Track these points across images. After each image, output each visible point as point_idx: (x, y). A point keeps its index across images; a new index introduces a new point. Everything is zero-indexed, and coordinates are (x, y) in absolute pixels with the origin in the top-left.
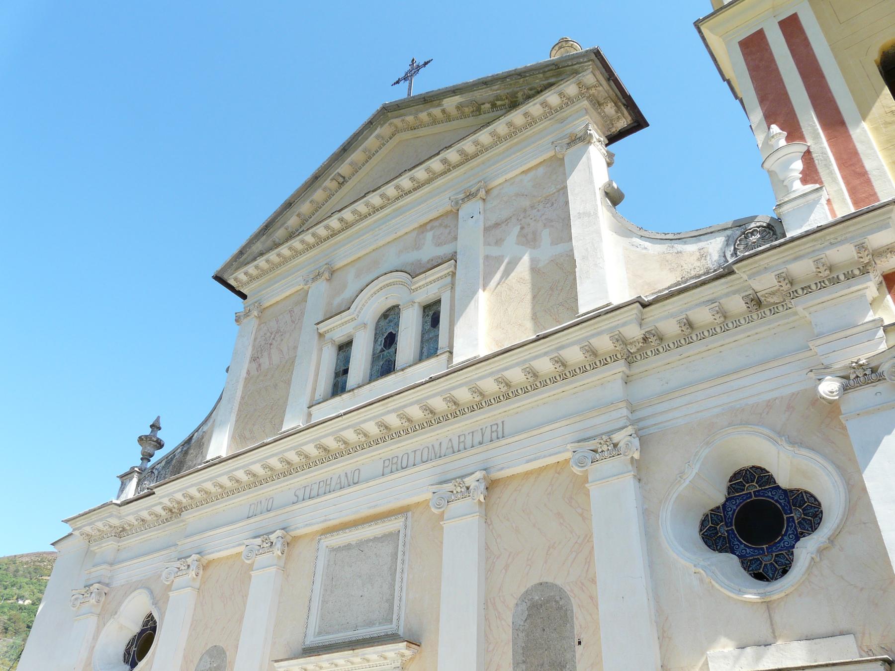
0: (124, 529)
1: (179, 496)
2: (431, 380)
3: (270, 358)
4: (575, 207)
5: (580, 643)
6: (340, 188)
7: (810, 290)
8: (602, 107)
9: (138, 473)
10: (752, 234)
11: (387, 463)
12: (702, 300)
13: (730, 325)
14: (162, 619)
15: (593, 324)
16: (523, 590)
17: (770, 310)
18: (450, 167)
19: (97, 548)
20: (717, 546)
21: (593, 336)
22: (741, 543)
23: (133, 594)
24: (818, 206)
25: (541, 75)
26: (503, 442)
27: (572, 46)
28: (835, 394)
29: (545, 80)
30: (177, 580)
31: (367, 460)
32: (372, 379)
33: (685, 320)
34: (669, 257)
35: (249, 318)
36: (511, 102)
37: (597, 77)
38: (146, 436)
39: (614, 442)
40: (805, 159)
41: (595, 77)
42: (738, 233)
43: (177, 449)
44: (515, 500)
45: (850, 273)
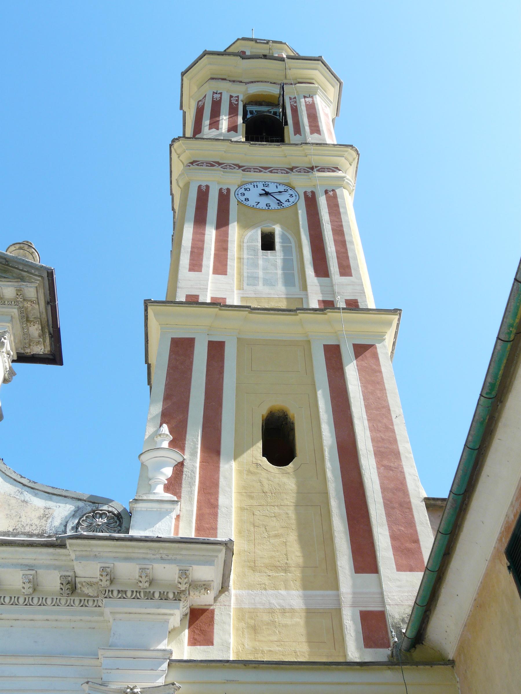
7: (124, 596)
8: (29, 324)
10: (101, 516)
12: (21, 561)
17: (81, 601)
24: (167, 517)
27: (32, 254)
34: (13, 501)
37: (39, 295)
42: (89, 509)
45: (165, 593)
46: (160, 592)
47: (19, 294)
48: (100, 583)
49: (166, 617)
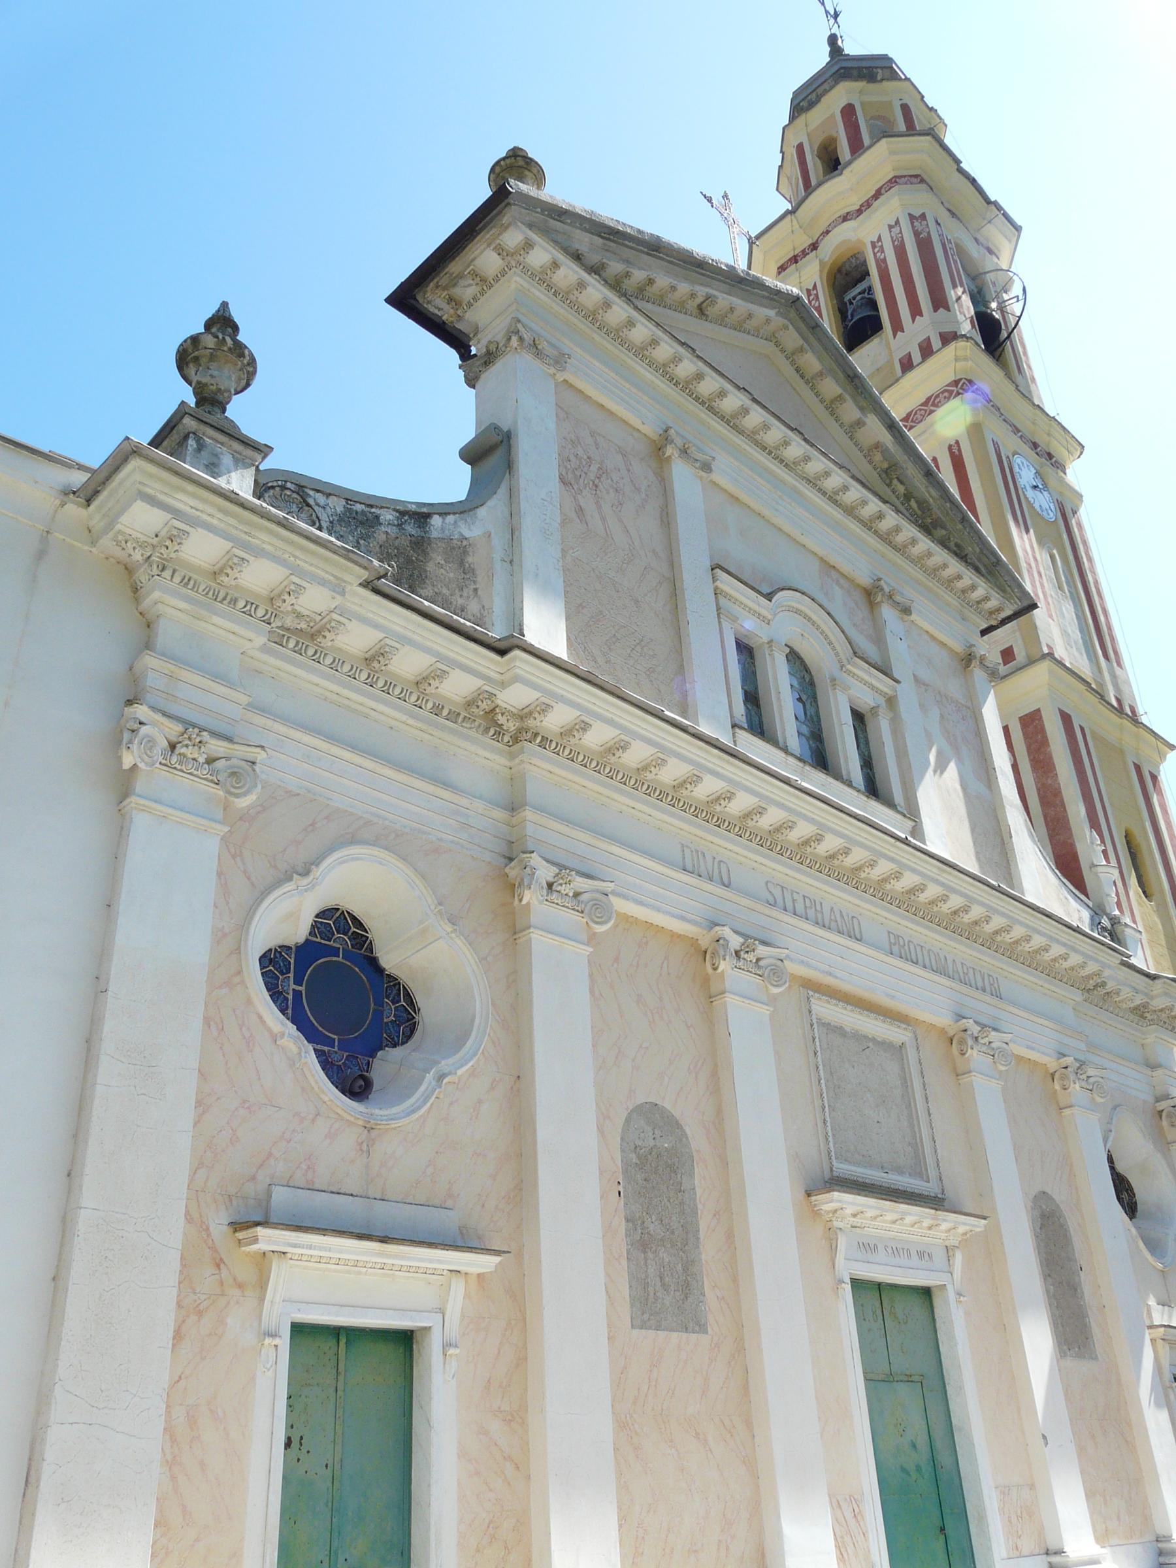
31: (868, 913)
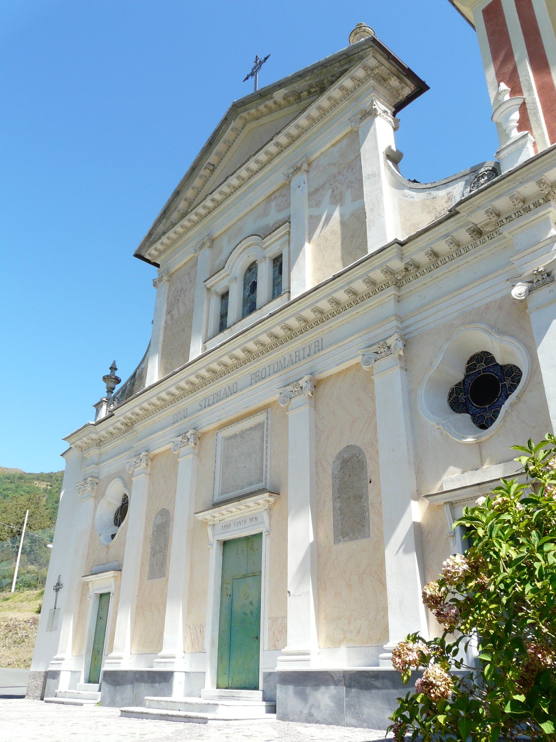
0: (101, 441)
1: (129, 415)
2: (271, 315)
3: (178, 310)
4: (366, 170)
5: (370, 482)
6: (212, 174)
7: (511, 219)
8: (387, 82)
9: (106, 402)
10: (482, 177)
11: (253, 376)
12: (440, 235)
13: (462, 251)
14: (130, 496)
15: (370, 263)
16: (338, 452)
17: (488, 236)
18: (282, 148)
19: (87, 454)
20: (458, 409)
21: (370, 271)
22: (473, 406)
23: (112, 482)
24: (525, 149)
25: (338, 64)
26: (322, 353)
27: (365, 31)
28: (523, 294)
29: (341, 68)
30: (136, 470)
31: (240, 376)
32: (244, 316)
33: (430, 252)
34: (428, 202)
35: (162, 282)
36: (321, 88)
37: (378, 59)
38: (107, 376)
39: (388, 345)
40: (522, 110)
41: (376, 59)
42: (473, 177)
43: (128, 382)
44: (332, 392)
45: (537, 202)
46: (533, 204)
47: (366, 69)
48: (491, 221)
49: (545, 216)
